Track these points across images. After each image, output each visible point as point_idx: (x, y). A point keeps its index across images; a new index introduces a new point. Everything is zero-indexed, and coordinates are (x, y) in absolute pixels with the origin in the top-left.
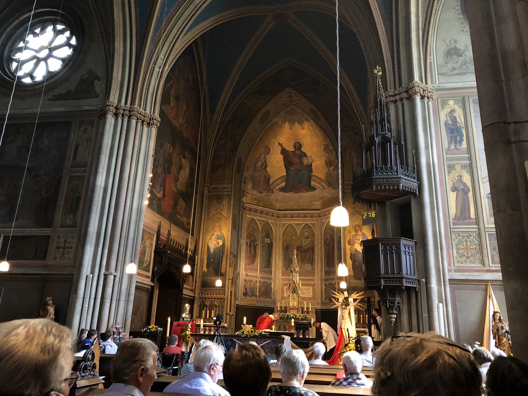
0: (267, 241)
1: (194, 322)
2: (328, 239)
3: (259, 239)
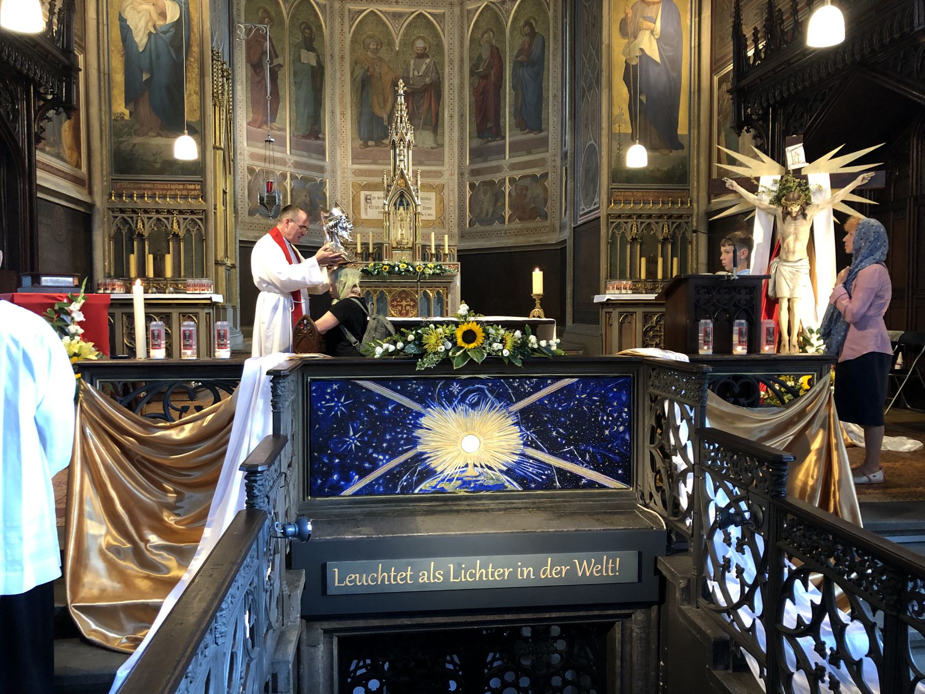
0: (309, 58)
1: (101, 291)
2: (484, 57)
3: (283, 48)
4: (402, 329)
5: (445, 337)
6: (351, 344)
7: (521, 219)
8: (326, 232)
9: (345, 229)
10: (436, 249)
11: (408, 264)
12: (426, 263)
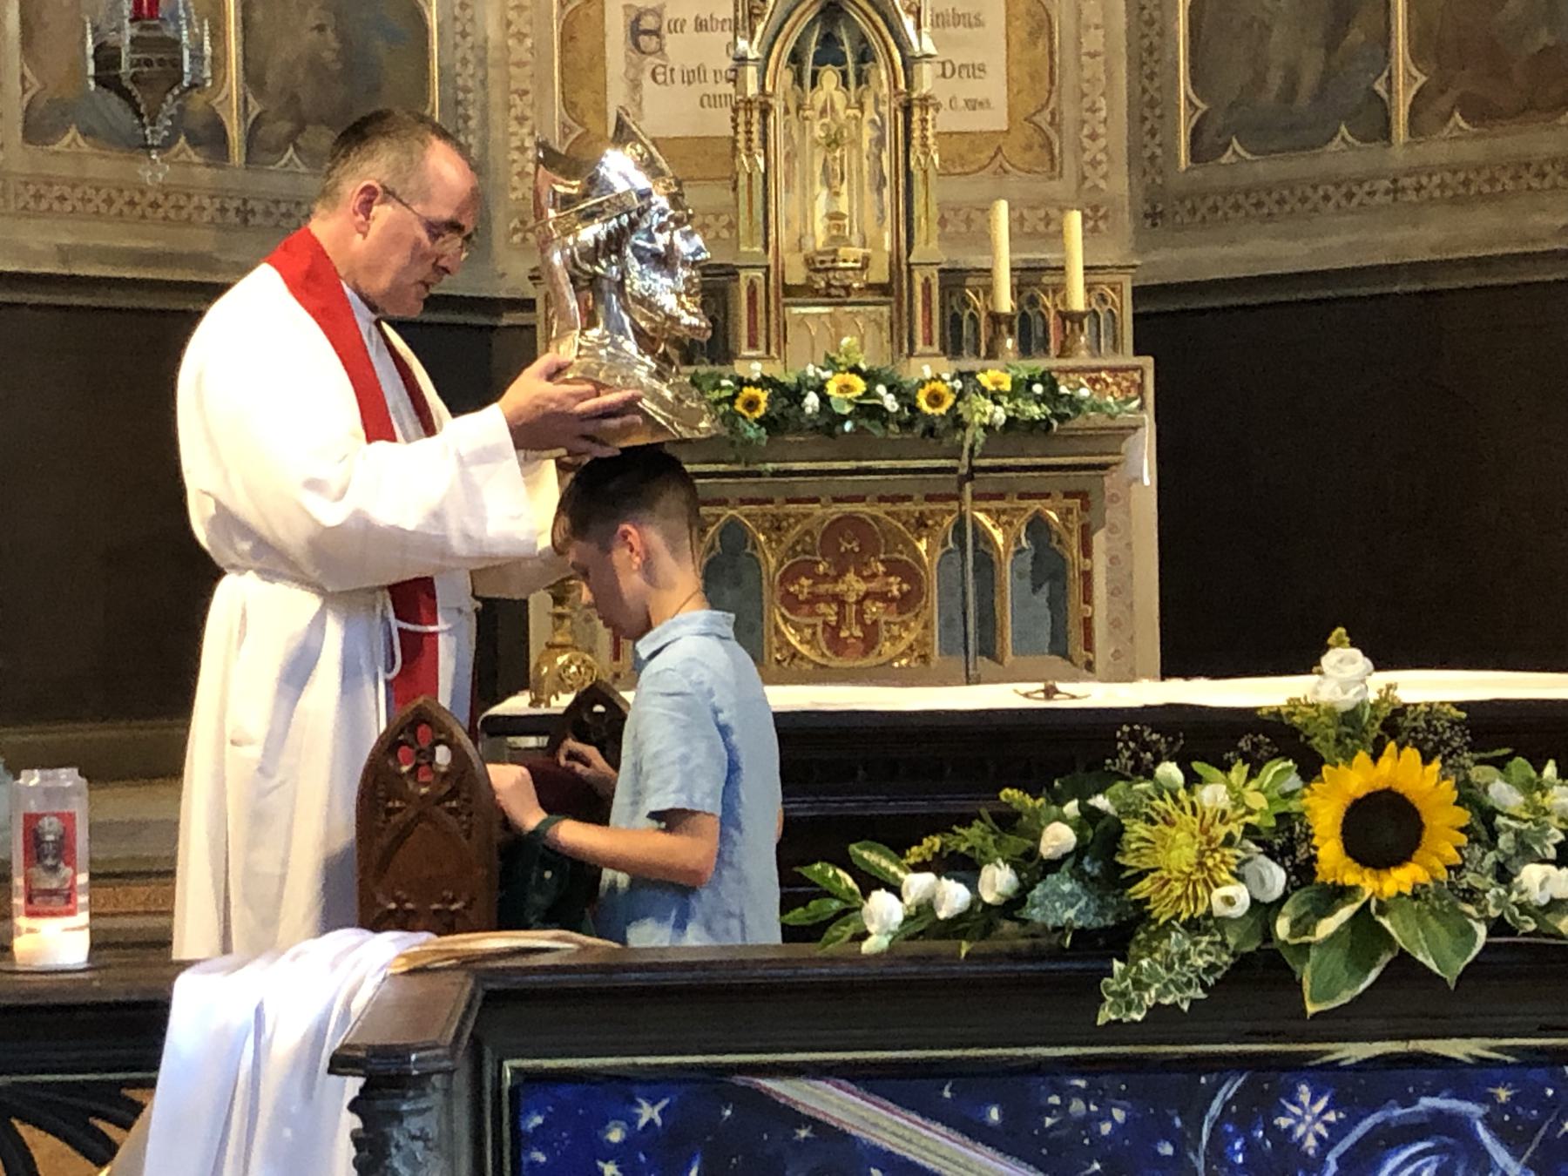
4: (1008, 794)
5: (1250, 831)
8: (563, 277)
9: (664, 261)
10: (1018, 290)
11: (870, 377)
12: (967, 364)
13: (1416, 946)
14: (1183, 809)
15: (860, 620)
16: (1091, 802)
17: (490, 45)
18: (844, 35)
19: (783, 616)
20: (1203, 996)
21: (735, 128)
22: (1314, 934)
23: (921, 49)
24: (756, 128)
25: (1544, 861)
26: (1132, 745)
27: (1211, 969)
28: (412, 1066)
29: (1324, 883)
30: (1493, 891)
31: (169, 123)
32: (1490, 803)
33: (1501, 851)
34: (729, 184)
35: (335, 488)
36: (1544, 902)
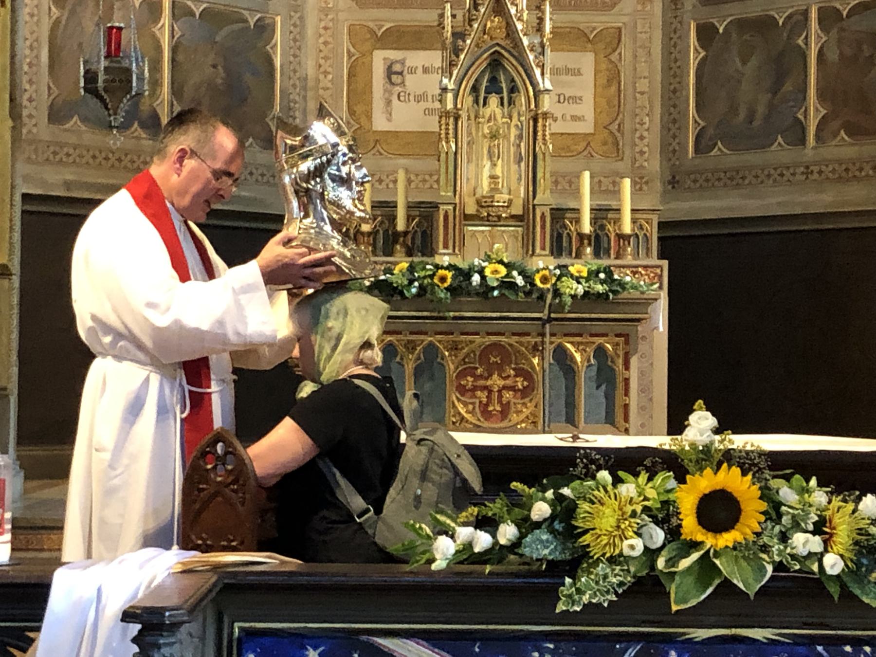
4: (515, 485)
5: (646, 509)
6: (348, 517)
7: (854, 131)
8: (290, 190)
9: (345, 181)
10: (594, 221)
11: (509, 266)
12: (564, 261)
13: (733, 576)
14: (609, 497)
15: (500, 402)
16: (561, 491)
17: (309, 77)
18: (502, 78)
19: (457, 398)
20: (615, 599)
21: (440, 126)
22: (677, 567)
23: (544, 87)
24: (451, 127)
25: (806, 531)
26: (585, 461)
27: (621, 584)
28: (166, 619)
29: (685, 539)
30: (776, 547)
31: (124, 114)
32: (780, 499)
33: (784, 526)
34: (437, 157)
35: (163, 307)
36: (805, 554)
